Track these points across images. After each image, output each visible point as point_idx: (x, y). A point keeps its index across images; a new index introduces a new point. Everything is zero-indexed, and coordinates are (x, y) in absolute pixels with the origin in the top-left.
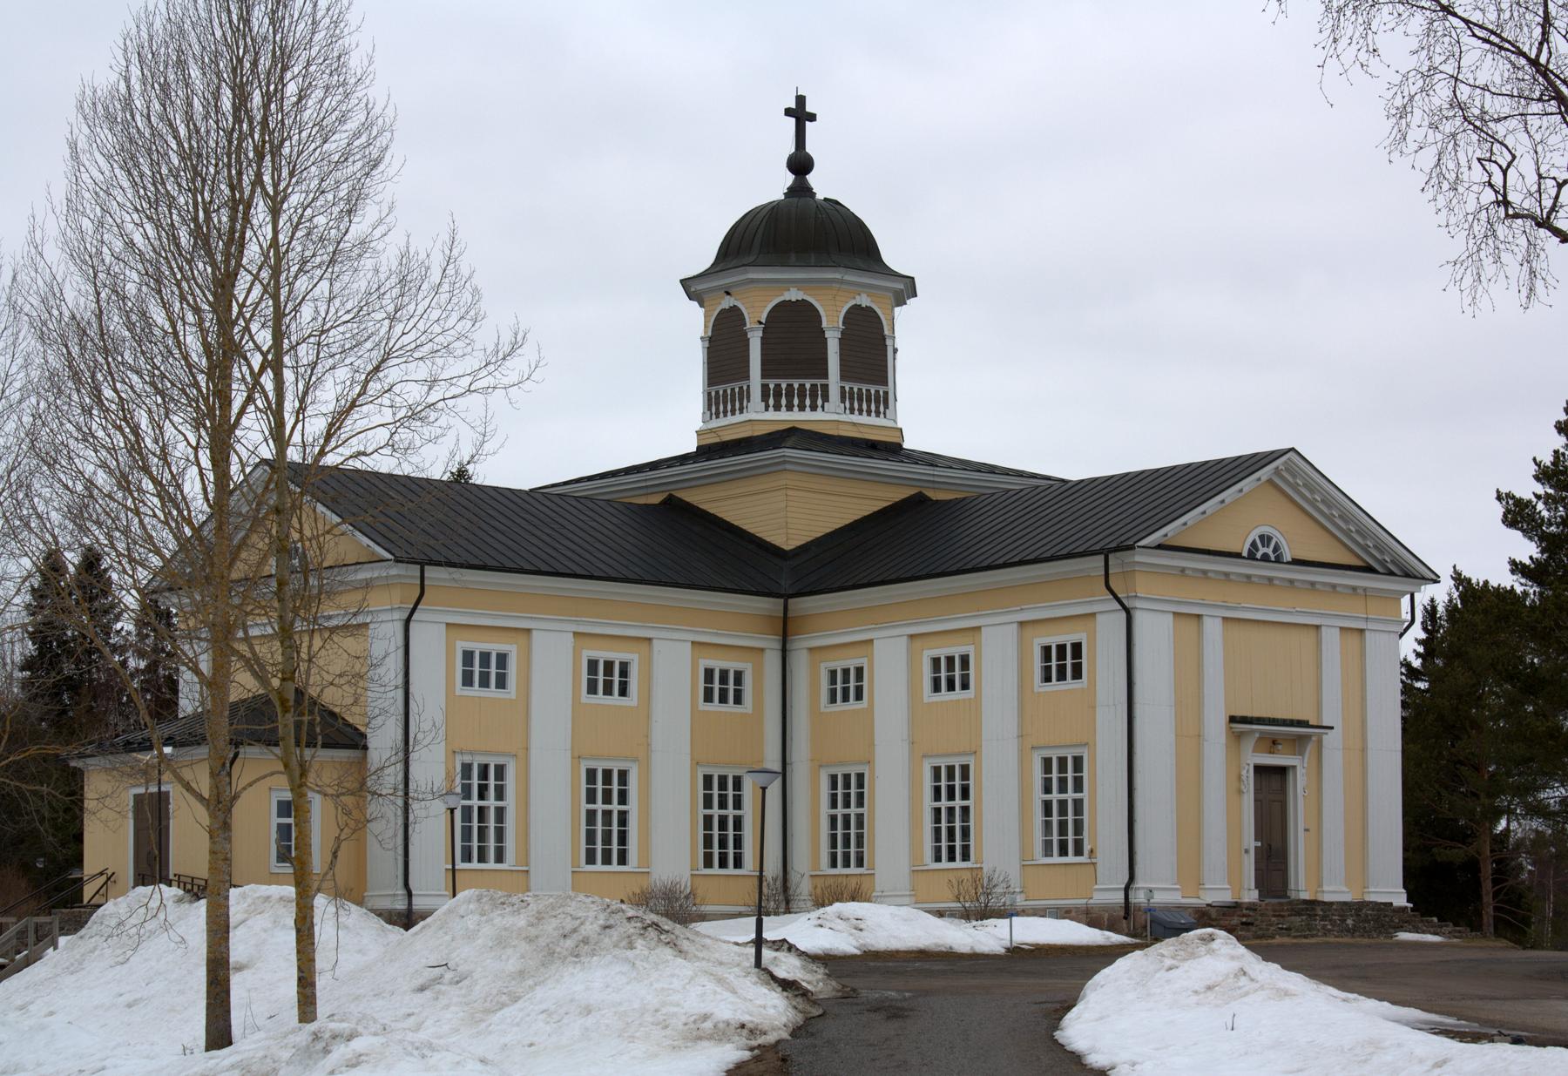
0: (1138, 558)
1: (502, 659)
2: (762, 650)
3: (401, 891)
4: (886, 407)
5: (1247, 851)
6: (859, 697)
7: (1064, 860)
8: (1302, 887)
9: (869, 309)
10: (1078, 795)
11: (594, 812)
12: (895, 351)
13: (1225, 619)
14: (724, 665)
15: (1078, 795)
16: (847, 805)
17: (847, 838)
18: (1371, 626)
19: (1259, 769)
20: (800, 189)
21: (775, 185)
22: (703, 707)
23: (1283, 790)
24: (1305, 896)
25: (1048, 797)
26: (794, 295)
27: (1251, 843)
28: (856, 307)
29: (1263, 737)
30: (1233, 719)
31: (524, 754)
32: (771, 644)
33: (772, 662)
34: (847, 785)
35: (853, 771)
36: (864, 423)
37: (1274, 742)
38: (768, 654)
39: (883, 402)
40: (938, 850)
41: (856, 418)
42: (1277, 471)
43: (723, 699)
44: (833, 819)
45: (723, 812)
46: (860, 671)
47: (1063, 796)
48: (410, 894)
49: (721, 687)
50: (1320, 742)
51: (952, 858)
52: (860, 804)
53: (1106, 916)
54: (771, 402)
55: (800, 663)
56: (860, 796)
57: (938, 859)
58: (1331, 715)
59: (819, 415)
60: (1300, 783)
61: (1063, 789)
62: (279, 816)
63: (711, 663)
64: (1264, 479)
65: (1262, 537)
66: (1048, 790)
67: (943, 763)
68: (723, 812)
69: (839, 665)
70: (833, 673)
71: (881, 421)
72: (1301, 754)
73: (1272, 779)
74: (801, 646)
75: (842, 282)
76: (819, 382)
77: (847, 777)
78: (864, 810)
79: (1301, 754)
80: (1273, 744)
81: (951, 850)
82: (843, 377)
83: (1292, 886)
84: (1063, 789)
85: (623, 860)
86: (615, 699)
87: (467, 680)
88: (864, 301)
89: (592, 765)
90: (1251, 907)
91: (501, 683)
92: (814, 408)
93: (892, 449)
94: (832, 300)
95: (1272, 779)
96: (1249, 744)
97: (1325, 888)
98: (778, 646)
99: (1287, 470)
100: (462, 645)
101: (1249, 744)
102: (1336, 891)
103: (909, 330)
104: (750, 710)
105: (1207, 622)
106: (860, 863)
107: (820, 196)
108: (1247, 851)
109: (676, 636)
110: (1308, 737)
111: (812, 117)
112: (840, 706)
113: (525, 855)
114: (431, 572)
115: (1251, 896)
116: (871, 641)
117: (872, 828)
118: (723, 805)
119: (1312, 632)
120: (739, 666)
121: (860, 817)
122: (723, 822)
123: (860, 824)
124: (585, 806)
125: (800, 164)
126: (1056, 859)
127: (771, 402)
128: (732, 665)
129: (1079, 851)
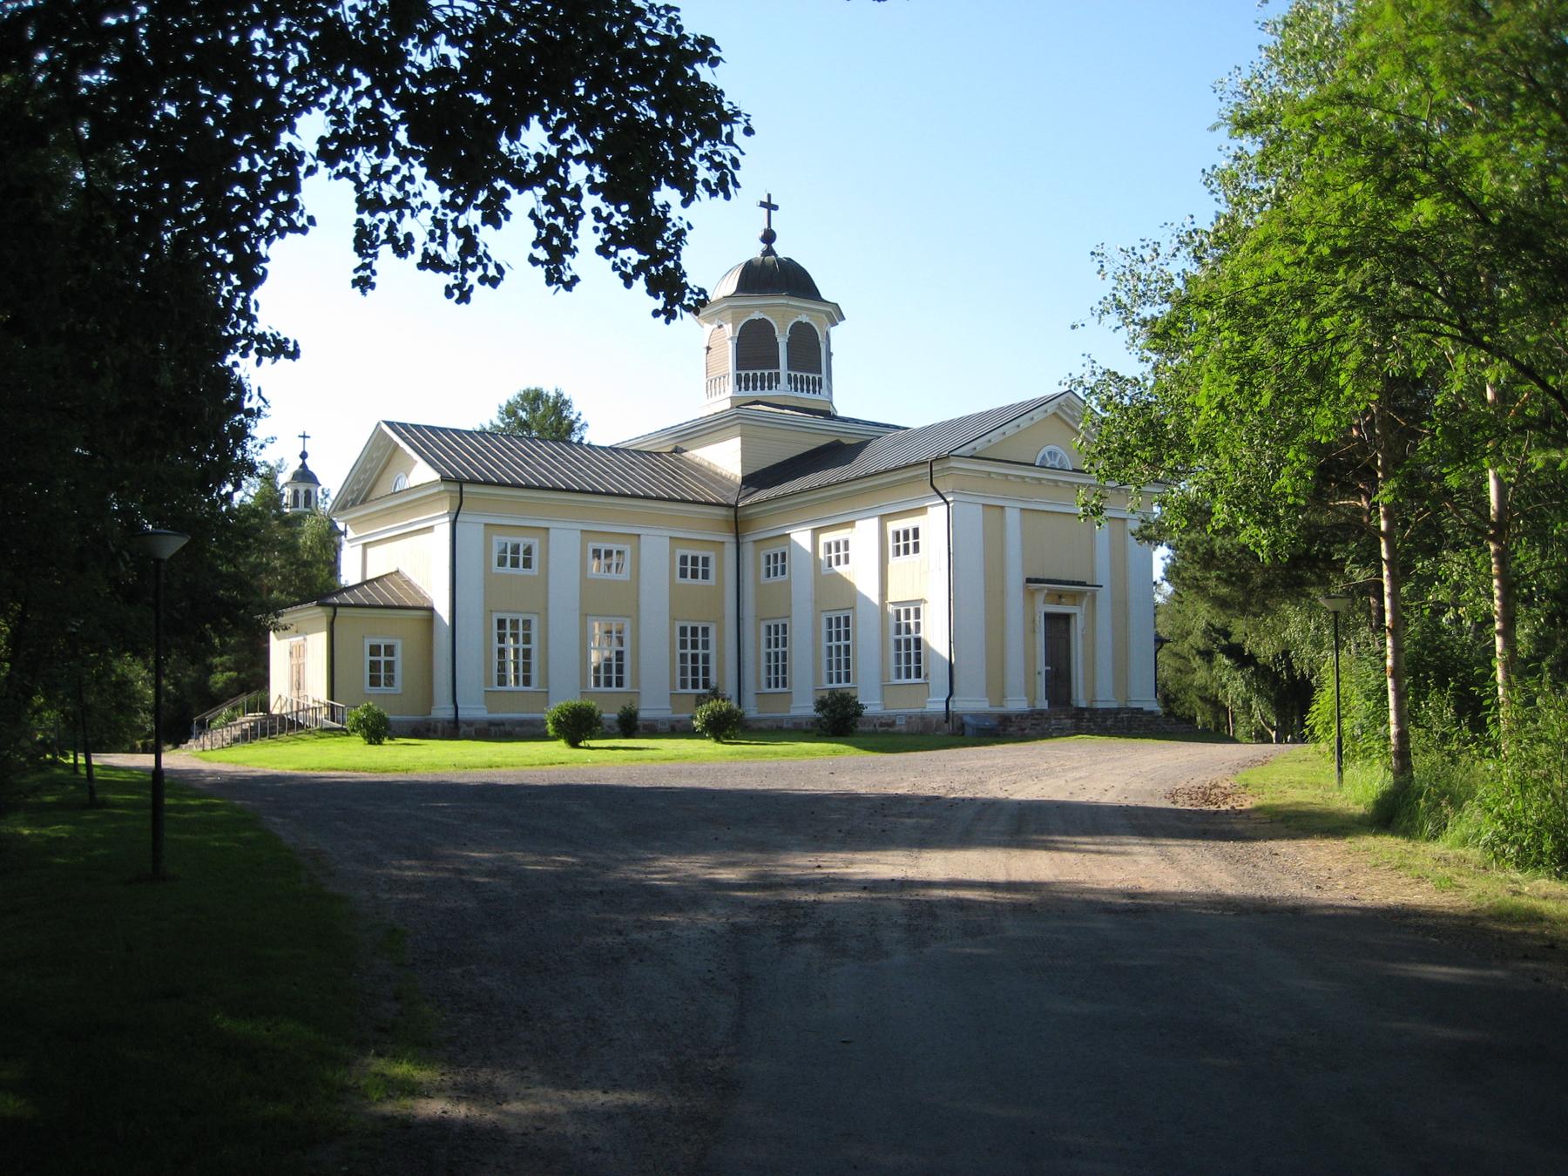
0: (952, 464)
1: (706, 561)
8: (1080, 699)
14: (695, 553)
16: (839, 639)
17: (908, 661)
19: (1048, 616)
20: (769, 251)
21: (755, 250)
22: (678, 580)
23: (1068, 630)
24: (1083, 704)
26: (756, 315)
27: (1041, 667)
28: (799, 323)
29: (1050, 593)
30: (1029, 580)
31: (544, 613)
32: (729, 539)
33: (730, 550)
35: (780, 622)
36: (807, 398)
38: (727, 546)
40: (899, 670)
41: (799, 394)
42: (1060, 406)
43: (694, 575)
44: (769, 655)
46: (784, 555)
49: (692, 567)
50: (1094, 596)
51: (908, 676)
56: (847, 632)
58: (1103, 575)
59: (773, 392)
60: (1078, 628)
64: (1050, 411)
65: (1050, 453)
66: (899, 632)
67: (833, 616)
69: (771, 552)
73: (1058, 626)
75: (788, 306)
77: (838, 619)
80: (1059, 598)
81: (908, 670)
85: (620, 683)
86: (521, 570)
87: (683, 574)
88: (804, 319)
89: (684, 624)
90: (1041, 713)
91: (706, 575)
92: (770, 388)
93: (829, 415)
94: (781, 314)
95: (1058, 626)
96: (1040, 597)
98: (733, 540)
100: (679, 553)
101: (1040, 597)
103: (840, 340)
106: (784, 685)
107: (297, 120)
109: (658, 532)
110: (1083, 594)
111: (776, 208)
114: (466, 488)
115: (1043, 704)
117: (855, 626)
119: (998, 511)
120: (706, 554)
121: (784, 653)
122: (695, 658)
123: (784, 659)
124: (496, 645)
125: (769, 237)
126: (904, 680)
128: (701, 554)
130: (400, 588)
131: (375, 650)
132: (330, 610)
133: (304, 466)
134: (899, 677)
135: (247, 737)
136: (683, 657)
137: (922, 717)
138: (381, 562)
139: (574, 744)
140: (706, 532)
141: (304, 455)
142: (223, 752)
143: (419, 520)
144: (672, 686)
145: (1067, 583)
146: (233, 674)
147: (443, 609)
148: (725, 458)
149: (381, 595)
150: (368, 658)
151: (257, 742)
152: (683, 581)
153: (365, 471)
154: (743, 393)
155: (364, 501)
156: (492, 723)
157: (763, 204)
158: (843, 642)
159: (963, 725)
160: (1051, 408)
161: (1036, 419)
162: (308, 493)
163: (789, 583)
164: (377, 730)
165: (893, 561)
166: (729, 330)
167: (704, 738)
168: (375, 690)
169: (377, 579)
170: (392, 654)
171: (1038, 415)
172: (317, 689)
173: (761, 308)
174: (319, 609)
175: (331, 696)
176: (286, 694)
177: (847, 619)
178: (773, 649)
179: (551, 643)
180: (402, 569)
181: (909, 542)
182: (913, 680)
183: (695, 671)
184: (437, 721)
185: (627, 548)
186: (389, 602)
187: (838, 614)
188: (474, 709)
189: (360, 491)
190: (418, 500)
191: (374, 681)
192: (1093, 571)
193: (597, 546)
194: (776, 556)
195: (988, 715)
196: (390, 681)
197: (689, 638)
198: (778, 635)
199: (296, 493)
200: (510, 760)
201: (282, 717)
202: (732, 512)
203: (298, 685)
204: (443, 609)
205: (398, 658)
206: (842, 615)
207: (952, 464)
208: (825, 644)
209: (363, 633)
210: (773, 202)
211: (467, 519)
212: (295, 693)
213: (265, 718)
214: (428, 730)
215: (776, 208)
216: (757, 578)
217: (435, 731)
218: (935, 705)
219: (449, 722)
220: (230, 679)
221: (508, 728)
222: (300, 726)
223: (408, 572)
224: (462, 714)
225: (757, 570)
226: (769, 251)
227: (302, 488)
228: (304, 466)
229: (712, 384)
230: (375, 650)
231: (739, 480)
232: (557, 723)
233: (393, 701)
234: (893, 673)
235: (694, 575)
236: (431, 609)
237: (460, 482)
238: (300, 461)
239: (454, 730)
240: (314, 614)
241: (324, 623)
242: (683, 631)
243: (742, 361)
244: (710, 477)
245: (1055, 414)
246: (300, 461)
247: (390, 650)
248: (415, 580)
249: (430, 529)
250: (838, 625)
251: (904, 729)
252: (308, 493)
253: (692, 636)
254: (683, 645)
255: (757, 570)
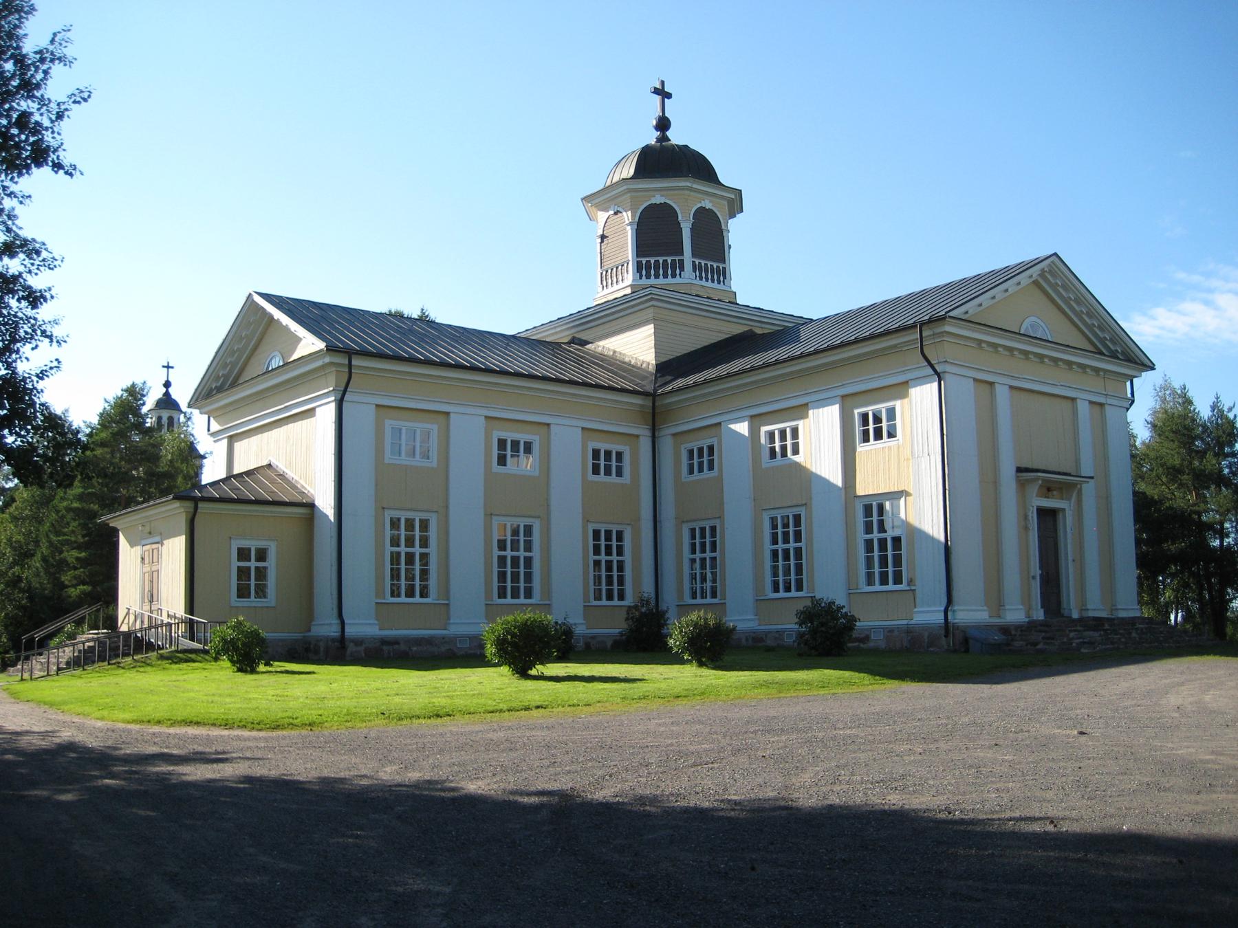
0: (947, 328)
1: (619, 455)
2: (638, 436)
3: (336, 621)
4: (725, 278)
5: (1034, 578)
6: (711, 468)
7: (884, 588)
9: (710, 211)
10: (798, 545)
11: (505, 557)
12: (730, 247)
13: (1011, 387)
14: (608, 447)
15: (798, 545)
18: (1109, 401)
20: (663, 138)
21: (651, 137)
24: (1075, 615)
25: (775, 547)
26: (658, 199)
30: (1019, 470)
32: (644, 432)
34: (703, 536)
37: (1049, 490)
39: (722, 275)
41: (703, 283)
42: (1042, 274)
45: (609, 558)
46: (711, 449)
47: (786, 546)
48: (343, 624)
50: (1080, 491)
52: (714, 549)
53: (926, 634)
54: (644, 273)
55: (666, 445)
56: (714, 544)
57: (776, 590)
58: (1086, 470)
59: (678, 280)
60: (1068, 522)
61: (786, 541)
62: (265, 568)
63: (597, 445)
64: (1023, 283)
66: (775, 542)
68: (609, 558)
69: (695, 445)
70: (691, 452)
71: (721, 286)
72: (1069, 499)
73: (1048, 517)
74: (666, 432)
76: (677, 258)
77: (703, 530)
78: (802, 544)
79: (1069, 499)
82: (694, 255)
83: (1064, 605)
84: (786, 541)
87: (596, 470)
88: (708, 206)
89: (597, 526)
91: (619, 473)
92: (674, 276)
94: (685, 199)
97: (1089, 607)
98: (649, 433)
99: (1050, 272)
101: (1034, 489)
102: (1096, 607)
103: (737, 231)
104: (628, 481)
105: (998, 388)
108: (1034, 578)
109: (568, 422)
111: (669, 96)
112: (697, 476)
113: (446, 591)
115: (1039, 615)
116: (720, 424)
117: (723, 537)
118: (609, 553)
119: (1069, 403)
120: (620, 448)
123: (714, 566)
125: (663, 124)
127: (644, 273)
128: (614, 448)
129: (898, 579)
130: (273, 482)
131: (243, 554)
132: (189, 505)
133: (167, 394)
134: (776, 590)
135: (82, 661)
136: (597, 564)
137: (909, 631)
138: (249, 455)
139: (523, 673)
140: (620, 422)
141: (167, 384)
142: (43, 684)
143: (298, 403)
144: (586, 599)
145: (1059, 473)
146: (87, 588)
147: (325, 503)
148: (637, 346)
149: (251, 490)
150: (235, 564)
151: (90, 668)
152: (596, 478)
153: (226, 365)
154: (644, 281)
155: (234, 384)
156: (384, 642)
157: (657, 91)
158: (792, 545)
159: (966, 640)
160: (1035, 271)
161: (1011, 291)
162: (171, 419)
163: (720, 479)
164: (248, 654)
165: (862, 449)
166: (627, 216)
167: (682, 662)
168: (244, 602)
169: (249, 473)
170: (240, 569)
171: (1024, 279)
172: (173, 602)
173: (660, 191)
174: (177, 504)
175: (190, 608)
176: (136, 608)
177: (713, 529)
178: (698, 555)
179: (452, 545)
180: (275, 462)
181: (878, 429)
182: (891, 586)
183: (883, 561)
184: (318, 639)
185: (536, 439)
186: (257, 497)
187: (702, 524)
188: (363, 626)
189: (226, 377)
190: (299, 378)
191: (243, 592)
192: (1077, 462)
193: (503, 435)
194: (701, 450)
195: (988, 627)
196: (261, 591)
197: (603, 543)
198: (706, 540)
199: (160, 419)
200: (460, 702)
201: (127, 635)
202: (648, 402)
203: (151, 597)
204: (325, 503)
205: (271, 563)
206: (791, 513)
207: (947, 328)
208: (768, 547)
209: (231, 534)
210: (658, 98)
211: (356, 398)
212: (147, 607)
213: (108, 636)
214: (307, 650)
215: (669, 96)
216: (677, 474)
217: (316, 652)
218: (928, 614)
219: (333, 640)
220: (83, 592)
221: (403, 647)
222: (151, 647)
223: (281, 465)
224: (350, 631)
225: (677, 463)
226: (663, 138)
227: (165, 414)
228: (167, 394)
229: (608, 274)
230: (243, 554)
231: (652, 368)
232: (501, 643)
233: (263, 615)
234: (862, 579)
235: (608, 472)
236: (311, 506)
237: (349, 353)
238: (164, 390)
239: (339, 651)
240: (173, 511)
241: (182, 522)
242: (596, 534)
243: (642, 247)
244: (614, 364)
245: (1036, 283)
246: (164, 390)
247: (262, 555)
248: (291, 474)
249: (310, 413)
250: (703, 536)
251: (883, 645)
252: (171, 419)
253: (606, 543)
254: (597, 550)
255: (677, 463)
